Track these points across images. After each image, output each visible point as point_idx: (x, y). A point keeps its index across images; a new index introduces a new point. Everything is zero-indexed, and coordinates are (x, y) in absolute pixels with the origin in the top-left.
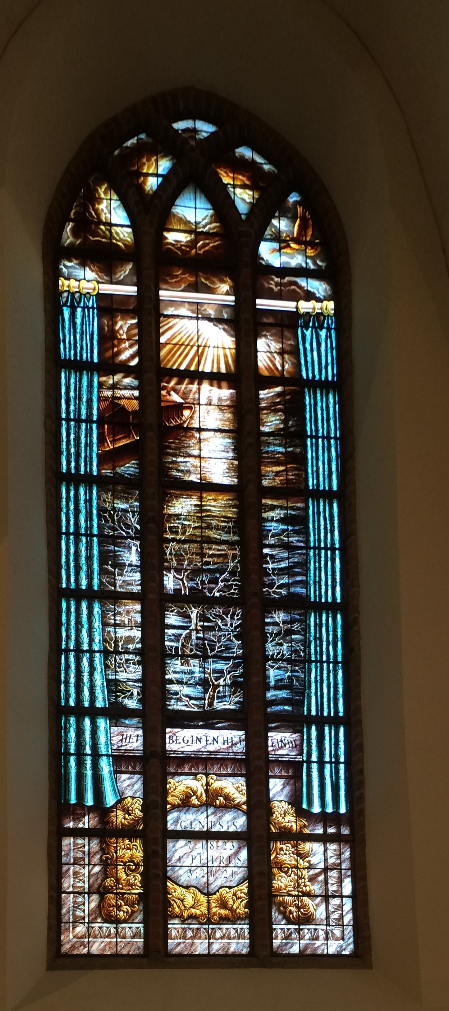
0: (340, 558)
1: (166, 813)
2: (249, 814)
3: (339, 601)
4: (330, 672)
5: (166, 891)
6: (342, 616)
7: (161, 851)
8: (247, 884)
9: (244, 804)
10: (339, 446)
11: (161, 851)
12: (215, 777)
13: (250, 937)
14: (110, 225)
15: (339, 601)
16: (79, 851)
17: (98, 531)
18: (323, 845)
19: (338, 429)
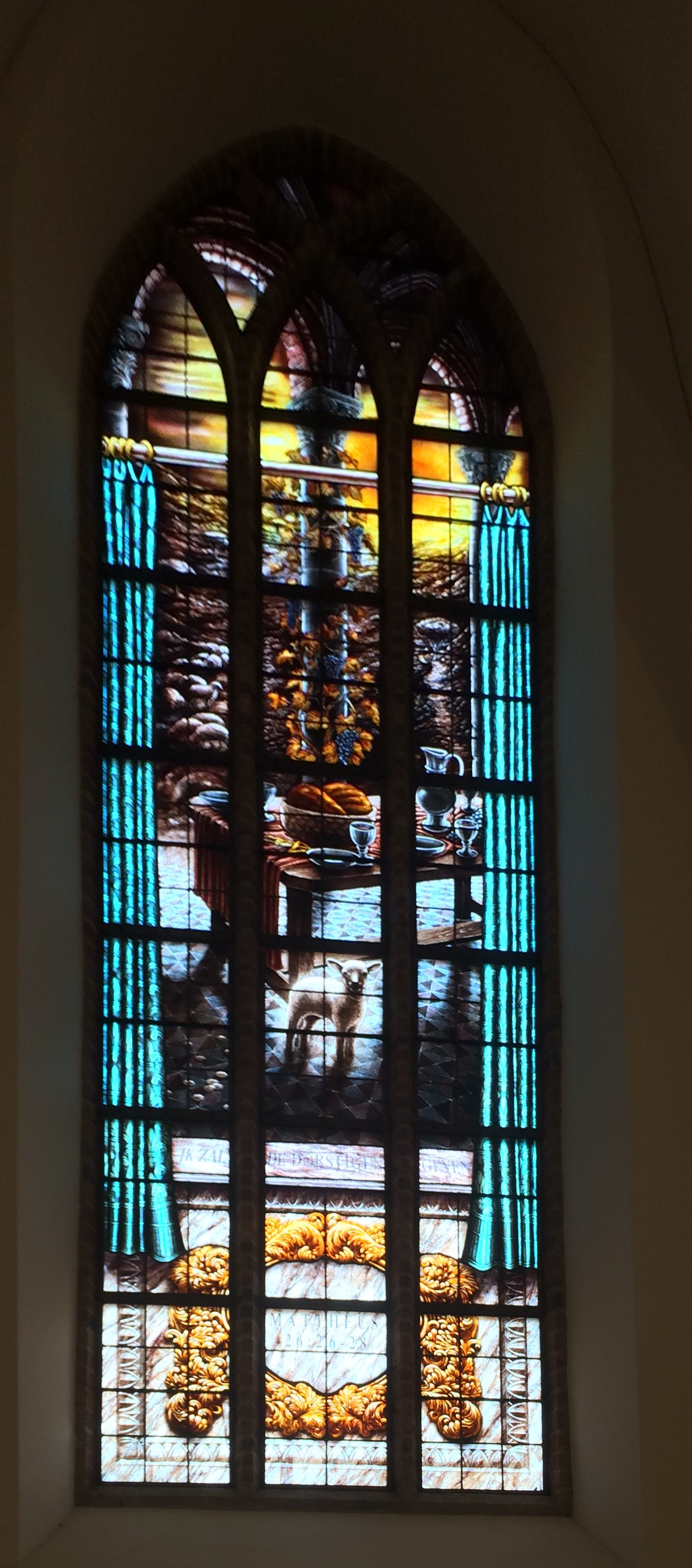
0: (536, 1007)
1: (262, 1270)
2: (389, 1275)
3: (530, 780)
4: (513, 1096)
5: (263, 1391)
6: (532, 707)
7: (255, 1242)
8: (385, 1381)
9: (382, 1258)
10: (534, 1089)
11: (255, 1242)
12: (336, 1216)
13: (385, 1154)
14: (188, 1215)
15: (530, 780)
16: (133, 1262)
17: (165, 1097)
18: (498, 1322)
19: (533, 906)
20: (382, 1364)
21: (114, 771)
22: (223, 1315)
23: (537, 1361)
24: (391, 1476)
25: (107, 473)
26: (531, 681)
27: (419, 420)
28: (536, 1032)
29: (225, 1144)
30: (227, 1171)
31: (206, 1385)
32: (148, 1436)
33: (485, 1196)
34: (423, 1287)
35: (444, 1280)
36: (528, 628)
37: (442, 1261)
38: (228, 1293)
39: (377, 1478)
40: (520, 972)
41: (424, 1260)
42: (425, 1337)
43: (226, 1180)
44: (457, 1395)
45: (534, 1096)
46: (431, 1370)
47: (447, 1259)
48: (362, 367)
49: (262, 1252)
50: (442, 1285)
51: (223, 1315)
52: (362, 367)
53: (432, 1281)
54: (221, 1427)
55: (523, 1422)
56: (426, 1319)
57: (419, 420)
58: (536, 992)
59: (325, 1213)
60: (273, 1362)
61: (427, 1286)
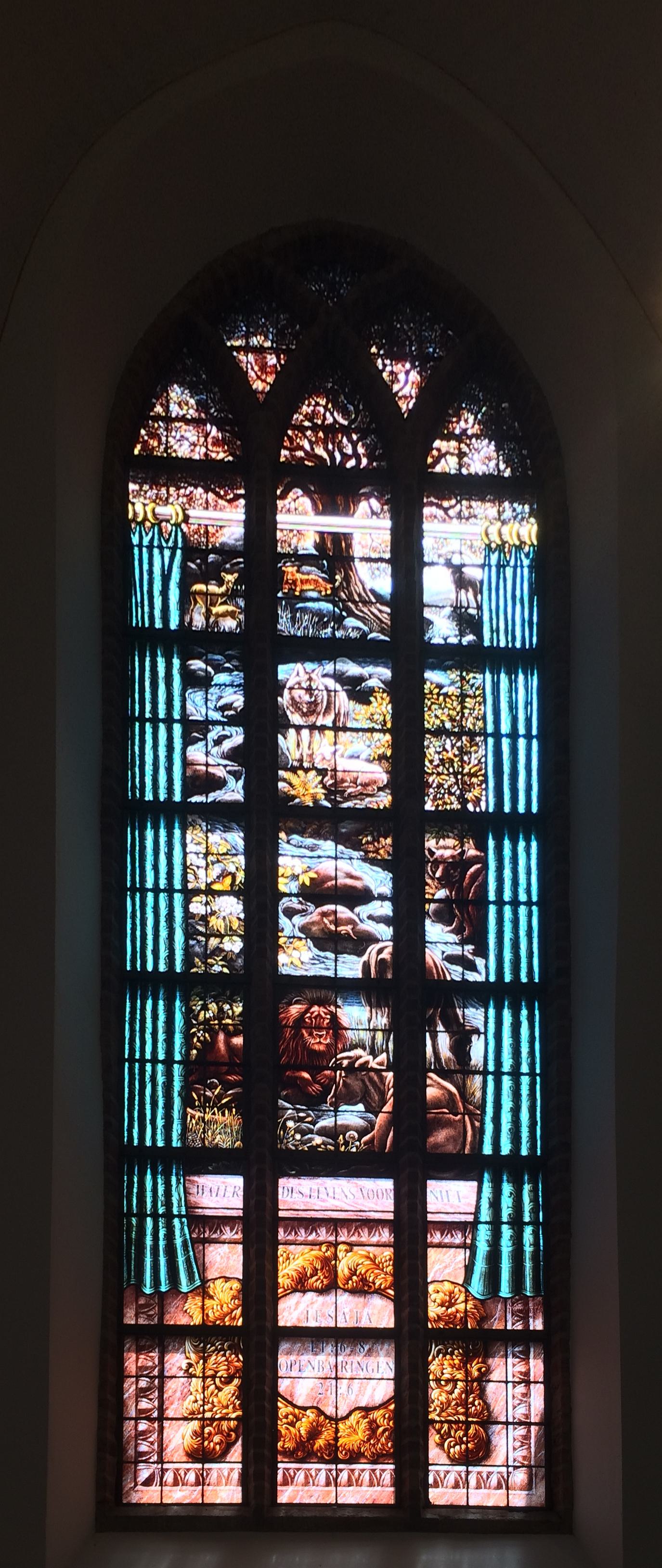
0: (539, 1009)
3: (537, 980)
25: (135, 540)
26: (537, 605)
27: (151, 799)
28: (539, 746)
30: (240, 1205)
31: (481, 519)
35: (451, 1305)
37: (447, 1286)
39: (384, 1494)
41: (431, 1288)
42: (464, 1022)
43: (240, 1213)
44: (462, 1418)
46: (436, 1395)
47: (453, 1286)
49: (276, 1285)
53: (440, 1307)
54: (236, 1452)
55: (527, 1443)
57: (151, 799)
60: (283, 1386)
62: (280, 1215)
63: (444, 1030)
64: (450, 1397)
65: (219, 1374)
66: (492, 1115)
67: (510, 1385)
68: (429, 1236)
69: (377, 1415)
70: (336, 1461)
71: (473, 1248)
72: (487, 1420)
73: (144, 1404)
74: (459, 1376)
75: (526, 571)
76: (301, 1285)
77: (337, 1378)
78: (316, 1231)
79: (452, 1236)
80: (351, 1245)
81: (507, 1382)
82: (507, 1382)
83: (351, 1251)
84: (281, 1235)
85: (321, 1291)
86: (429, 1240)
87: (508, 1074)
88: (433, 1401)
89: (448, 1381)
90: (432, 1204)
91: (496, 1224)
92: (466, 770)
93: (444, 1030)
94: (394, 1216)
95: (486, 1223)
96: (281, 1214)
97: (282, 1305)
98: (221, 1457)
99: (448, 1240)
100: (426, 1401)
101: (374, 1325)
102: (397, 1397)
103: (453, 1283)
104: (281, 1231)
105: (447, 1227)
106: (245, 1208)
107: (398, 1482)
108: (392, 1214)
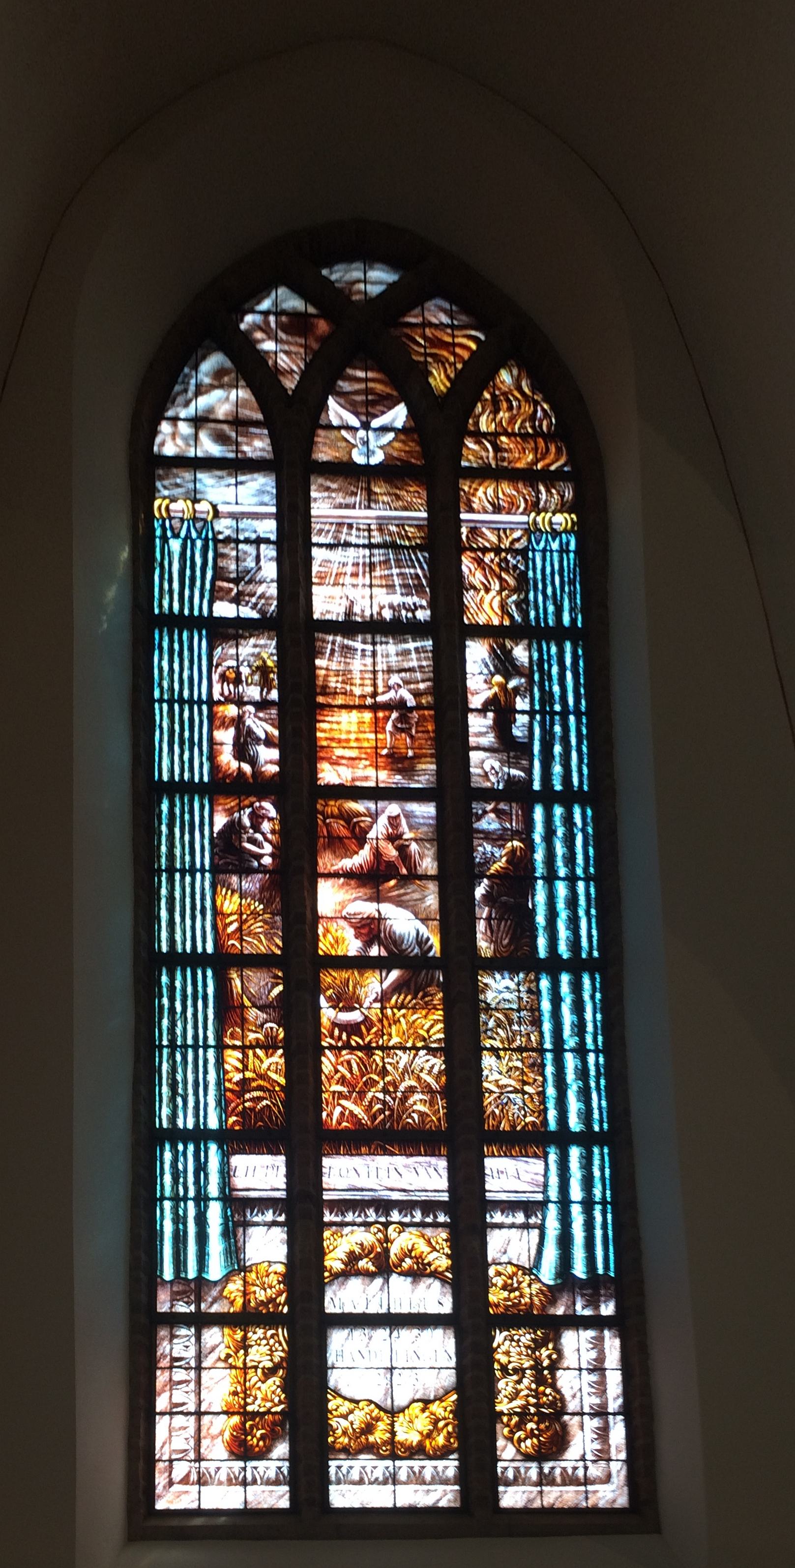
20: (449, 1378)
21: (554, 650)
22: (283, 1333)
23: (620, 1463)
24: (464, 1494)
29: (281, 1160)
32: (204, 1460)
33: (555, 1202)
34: (492, 1298)
36: (157, 1126)
38: (285, 1310)
40: (593, 1354)
41: (491, 1272)
45: (578, 596)
46: (505, 1386)
48: (581, 643)
50: (512, 1295)
51: (283, 1333)
52: (581, 643)
56: (498, 1331)
58: (589, 775)
59: (386, 1225)
60: (335, 1379)
61: (496, 1296)
62: (325, 1197)
63: (420, 308)
64: (518, 1387)
65: (261, 1366)
66: (563, 1004)
67: (584, 1372)
68: (488, 1216)
69: (436, 1408)
70: (394, 1457)
71: (542, 1228)
72: (559, 1408)
73: (178, 1397)
74: (526, 1365)
75: (572, 555)
76: (351, 1269)
77: (391, 1369)
78: (592, 1349)
79: (514, 1216)
80: (403, 1225)
81: (580, 1369)
82: (580, 1369)
83: (404, 1231)
84: (328, 1217)
85: (370, 1275)
86: (488, 1220)
87: (572, 1050)
88: (500, 1392)
89: (516, 1371)
90: (491, 1184)
91: (565, 1203)
92: (506, 544)
93: (420, 308)
94: (449, 1197)
95: (555, 1202)
96: (327, 1196)
97: (329, 1294)
98: (263, 1455)
99: (509, 1220)
100: (492, 1394)
101: (414, 1311)
102: (459, 1387)
103: (515, 1265)
104: (327, 1213)
105: (509, 1206)
106: (289, 1188)
107: (462, 1478)
108: (447, 1194)
